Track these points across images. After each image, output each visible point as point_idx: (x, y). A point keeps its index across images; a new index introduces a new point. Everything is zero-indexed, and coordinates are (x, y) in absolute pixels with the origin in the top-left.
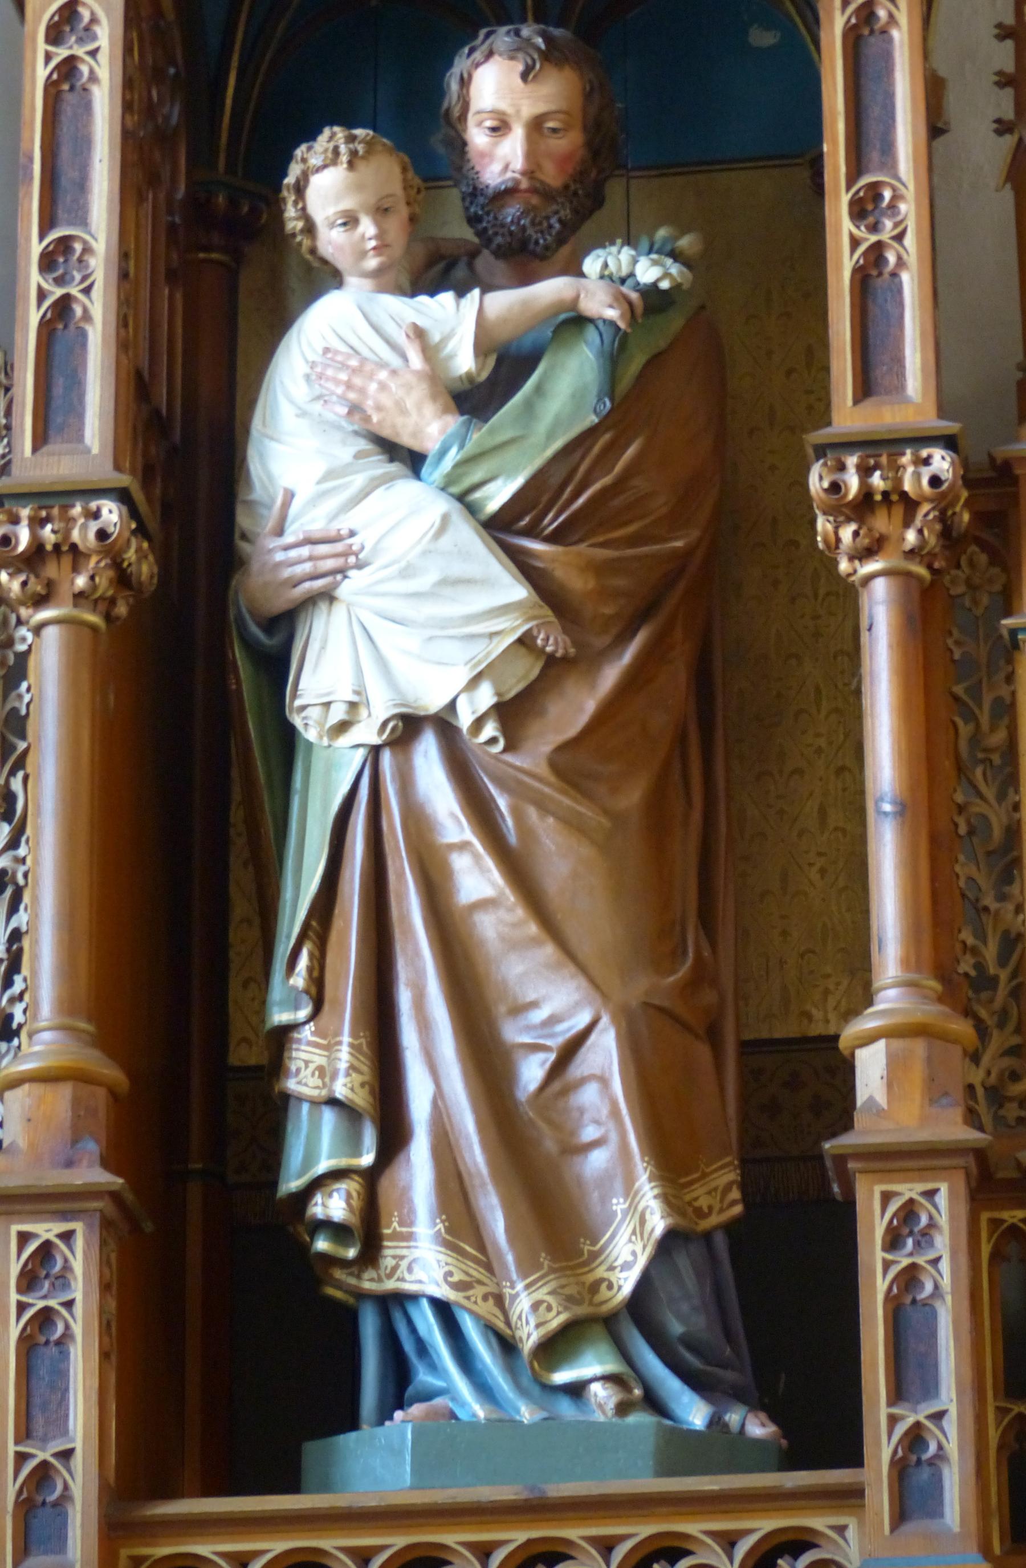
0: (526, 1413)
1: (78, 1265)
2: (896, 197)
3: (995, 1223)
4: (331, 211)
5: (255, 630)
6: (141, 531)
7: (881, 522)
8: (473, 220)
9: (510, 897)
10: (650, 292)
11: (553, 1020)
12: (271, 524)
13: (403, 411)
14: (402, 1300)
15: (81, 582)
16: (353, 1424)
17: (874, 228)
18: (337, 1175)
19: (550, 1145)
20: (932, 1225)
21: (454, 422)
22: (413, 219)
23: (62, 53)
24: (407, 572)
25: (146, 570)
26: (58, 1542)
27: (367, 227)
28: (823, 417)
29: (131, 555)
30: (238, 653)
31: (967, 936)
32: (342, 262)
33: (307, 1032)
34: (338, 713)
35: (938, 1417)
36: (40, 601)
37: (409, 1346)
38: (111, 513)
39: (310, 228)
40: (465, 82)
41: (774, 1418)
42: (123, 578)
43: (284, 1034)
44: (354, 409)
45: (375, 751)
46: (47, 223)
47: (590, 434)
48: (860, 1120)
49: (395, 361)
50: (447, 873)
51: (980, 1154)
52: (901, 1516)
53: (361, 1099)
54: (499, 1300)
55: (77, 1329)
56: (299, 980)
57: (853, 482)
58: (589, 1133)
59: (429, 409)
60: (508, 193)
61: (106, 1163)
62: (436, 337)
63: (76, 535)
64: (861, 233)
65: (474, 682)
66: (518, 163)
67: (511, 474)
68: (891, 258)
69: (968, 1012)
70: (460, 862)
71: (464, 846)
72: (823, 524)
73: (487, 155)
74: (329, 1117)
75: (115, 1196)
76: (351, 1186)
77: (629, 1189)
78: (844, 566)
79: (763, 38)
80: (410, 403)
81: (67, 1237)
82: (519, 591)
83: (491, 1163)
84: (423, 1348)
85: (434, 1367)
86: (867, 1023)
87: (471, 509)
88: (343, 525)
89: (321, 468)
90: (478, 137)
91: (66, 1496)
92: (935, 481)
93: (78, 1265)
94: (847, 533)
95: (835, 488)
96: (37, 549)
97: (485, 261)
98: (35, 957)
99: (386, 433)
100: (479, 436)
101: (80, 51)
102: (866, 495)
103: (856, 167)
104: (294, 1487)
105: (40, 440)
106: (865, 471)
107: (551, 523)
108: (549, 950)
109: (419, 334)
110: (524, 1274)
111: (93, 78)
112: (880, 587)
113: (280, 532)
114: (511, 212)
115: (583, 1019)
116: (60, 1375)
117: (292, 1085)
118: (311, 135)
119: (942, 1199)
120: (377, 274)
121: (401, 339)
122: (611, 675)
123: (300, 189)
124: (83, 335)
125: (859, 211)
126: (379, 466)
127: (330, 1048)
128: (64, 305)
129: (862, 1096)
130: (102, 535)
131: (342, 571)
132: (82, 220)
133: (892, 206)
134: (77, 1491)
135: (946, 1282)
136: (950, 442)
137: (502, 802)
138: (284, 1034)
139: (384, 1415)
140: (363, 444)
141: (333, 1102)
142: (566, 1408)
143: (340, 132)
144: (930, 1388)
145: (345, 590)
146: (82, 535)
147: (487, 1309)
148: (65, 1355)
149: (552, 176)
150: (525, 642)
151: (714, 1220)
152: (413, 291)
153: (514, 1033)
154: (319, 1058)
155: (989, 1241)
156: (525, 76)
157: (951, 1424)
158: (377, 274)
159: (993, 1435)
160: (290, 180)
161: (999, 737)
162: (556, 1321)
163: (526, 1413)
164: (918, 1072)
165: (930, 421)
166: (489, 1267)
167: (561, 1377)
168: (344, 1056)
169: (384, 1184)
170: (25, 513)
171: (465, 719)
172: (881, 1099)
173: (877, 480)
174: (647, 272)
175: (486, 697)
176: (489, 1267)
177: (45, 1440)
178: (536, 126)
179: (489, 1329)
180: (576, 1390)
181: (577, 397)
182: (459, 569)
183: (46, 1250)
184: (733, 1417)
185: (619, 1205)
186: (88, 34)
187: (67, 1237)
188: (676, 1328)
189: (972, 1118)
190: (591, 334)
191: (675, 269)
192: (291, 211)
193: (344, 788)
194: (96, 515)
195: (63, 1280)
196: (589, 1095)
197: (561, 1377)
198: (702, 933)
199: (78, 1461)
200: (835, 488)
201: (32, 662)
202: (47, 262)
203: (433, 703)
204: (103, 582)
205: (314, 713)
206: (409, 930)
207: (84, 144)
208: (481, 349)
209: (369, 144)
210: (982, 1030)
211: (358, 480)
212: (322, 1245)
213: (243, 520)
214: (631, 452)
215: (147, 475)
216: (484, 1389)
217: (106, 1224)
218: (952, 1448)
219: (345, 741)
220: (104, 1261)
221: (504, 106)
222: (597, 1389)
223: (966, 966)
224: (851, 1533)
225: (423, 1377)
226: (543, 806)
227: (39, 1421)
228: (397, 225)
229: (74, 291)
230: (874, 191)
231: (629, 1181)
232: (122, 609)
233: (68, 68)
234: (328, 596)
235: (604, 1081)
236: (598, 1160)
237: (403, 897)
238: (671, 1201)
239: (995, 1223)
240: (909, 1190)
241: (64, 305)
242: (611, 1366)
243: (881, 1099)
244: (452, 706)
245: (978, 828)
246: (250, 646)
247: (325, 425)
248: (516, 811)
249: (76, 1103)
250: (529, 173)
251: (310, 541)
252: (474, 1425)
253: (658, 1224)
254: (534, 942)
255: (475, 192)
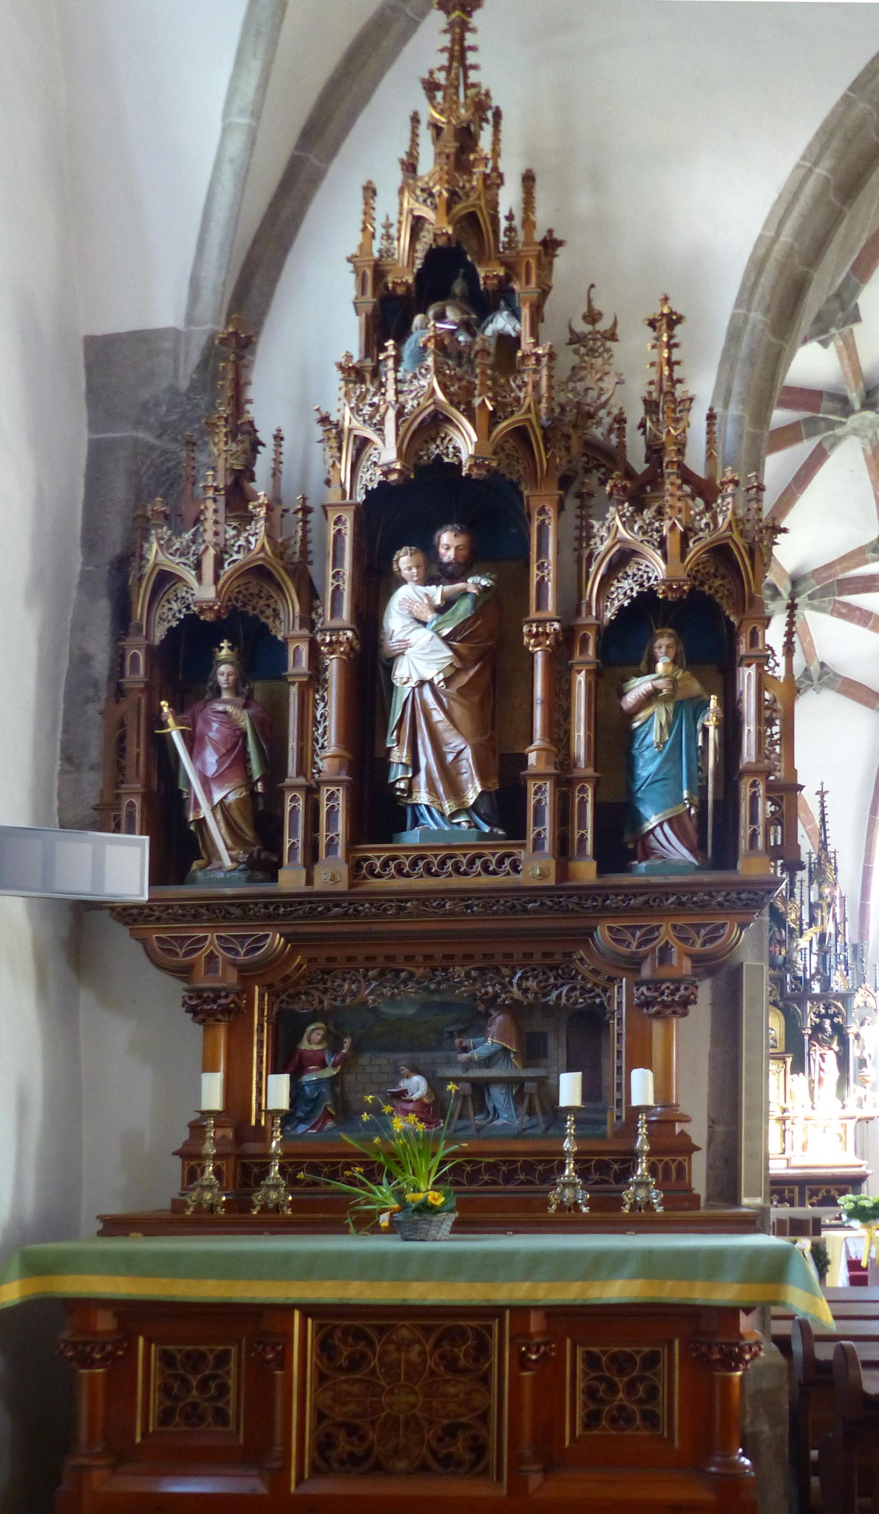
0: (446, 828)
1: (341, 796)
2: (548, 565)
3: (589, 1354)
4: (405, 566)
5: (385, 662)
6: (357, 639)
7: (541, 639)
8: (440, 570)
9: (446, 720)
10: (485, 586)
11: (456, 746)
12: (389, 638)
13: (422, 612)
14: (417, 805)
15: (342, 649)
16: (404, 830)
17: (543, 572)
18: (402, 779)
19: (454, 773)
20: (545, 790)
21: (435, 615)
22: (426, 569)
23: (338, 528)
24: (422, 649)
25: (358, 647)
26: (335, 852)
27: (414, 570)
28: (528, 614)
29: (354, 643)
30: (380, 667)
31: (556, 730)
32: (407, 578)
33: (396, 749)
34: (405, 680)
35: (544, 830)
36: (332, 653)
37: (418, 815)
38: (350, 634)
39: (400, 570)
40: (439, 537)
41: (504, 830)
42: (352, 649)
43: (390, 749)
44: (410, 612)
45: (414, 688)
46: (334, 567)
47: (469, 618)
48: (529, 768)
49: (419, 600)
50: (431, 714)
51: (557, 775)
52: (534, 849)
53: (409, 763)
54: (441, 805)
55: (340, 809)
56: (394, 737)
57: (534, 630)
58: (463, 770)
59: (429, 612)
60: (449, 564)
61: (348, 775)
62: (431, 596)
63: (341, 639)
64: (539, 573)
65: (438, 673)
66: (452, 557)
67: (448, 627)
68: (546, 579)
69: (556, 746)
70: (434, 713)
71: (435, 709)
72: (526, 639)
73: (444, 555)
74: (400, 766)
75: (349, 782)
76: (406, 781)
77: (473, 783)
78: (531, 649)
79: (514, 531)
80: (424, 610)
81: (338, 790)
82: (450, 653)
83: (440, 776)
84: (422, 815)
85: (424, 819)
86: (532, 748)
87: (439, 635)
88: (407, 638)
89: (402, 625)
90: (442, 550)
91: (337, 843)
92: (555, 630)
93: (341, 796)
94: (532, 641)
95: (530, 631)
96: (331, 642)
97: (443, 579)
98: (330, 731)
99: (418, 617)
100: (441, 618)
101: (342, 527)
102: (538, 632)
103: (539, 556)
104: (391, 842)
105: (332, 617)
106: (537, 627)
107: (459, 638)
108: (455, 731)
109: (427, 595)
110: (447, 799)
111: (345, 534)
112: (540, 653)
113: (391, 639)
114: (450, 568)
115: (463, 746)
116: (336, 820)
117: (392, 760)
118: (400, 548)
119: (341, 791)
120: (417, 581)
121: (422, 596)
122: (472, 672)
123: (397, 561)
124: (342, 594)
125: (539, 568)
126: (416, 625)
127: (401, 752)
128: (338, 587)
129: (530, 763)
130: (347, 639)
131: (406, 648)
132: (342, 566)
133: (547, 568)
134: (340, 843)
135: (548, 802)
136: (558, 621)
137: (444, 700)
138: (390, 749)
139: (412, 828)
140: (412, 620)
141: (402, 763)
142: (456, 827)
143: (408, 548)
144: (543, 823)
145: (407, 652)
146: (343, 638)
147: (438, 807)
148: (337, 815)
149: (460, 560)
150: (451, 665)
151: (492, 790)
152: (425, 585)
153: (446, 749)
154: (398, 754)
155: (480, 1325)
156: (455, 536)
157: (548, 831)
158: (417, 581)
159: (557, 834)
160: (395, 559)
161: (567, 686)
162: (454, 809)
163: (446, 828)
164: (543, 758)
165: (555, 616)
166: (438, 798)
167: (455, 821)
168: (405, 753)
169: (414, 781)
170: (328, 633)
171: (436, 681)
172: (535, 764)
173: (540, 629)
174: (484, 582)
175: (441, 676)
176: (438, 798)
177: (332, 832)
178: (457, 548)
179: (438, 811)
180: (459, 824)
181: (466, 610)
182: (435, 648)
183: (333, 793)
184: (495, 830)
185: (470, 786)
186: (344, 524)
187: (338, 790)
188: (483, 812)
189: (556, 768)
190: (470, 596)
191: (491, 582)
192: (395, 566)
193: (406, 696)
194: (346, 634)
195: (337, 799)
196: (464, 763)
197: (455, 821)
198: (316, 582)
199: (340, 836)
200: (530, 631)
201: (329, 668)
202: (334, 577)
203: (429, 678)
204: (347, 649)
205: (399, 680)
206: (421, 727)
207: (343, 549)
208: (442, 599)
209: (415, 551)
210: (559, 749)
211: (411, 628)
212: (398, 793)
213: (382, 637)
214: (479, 622)
215: (358, 626)
216: (436, 823)
217: (347, 788)
218: (547, 836)
219: (406, 686)
220: (347, 796)
221: (449, 543)
222: (464, 824)
223: (556, 736)
224: (523, 853)
225: (422, 821)
226: (453, 699)
227: (331, 828)
228: (421, 570)
229: (340, 583)
230: (543, 564)
231: (473, 780)
232: (352, 656)
233: (339, 531)
234: (403, 654)
235: (468, 760)
236: (465, 776)
237: (420, 720)
238: (482, 785)
239: (559, 791)
240: (540, 783)
241: (338, 587)
242: (467, 819)
243: (535, 764)
244: (432, 679)
245: (560, 707)
246: (383, 665)
247: (403, 616)
248: (448, 702)
249: (340, 762)
250: (455, 559)
251: (398, 641)
252: (434, 830)
253: (479, 790)
254: (451, 729)
255: (441, 563)
